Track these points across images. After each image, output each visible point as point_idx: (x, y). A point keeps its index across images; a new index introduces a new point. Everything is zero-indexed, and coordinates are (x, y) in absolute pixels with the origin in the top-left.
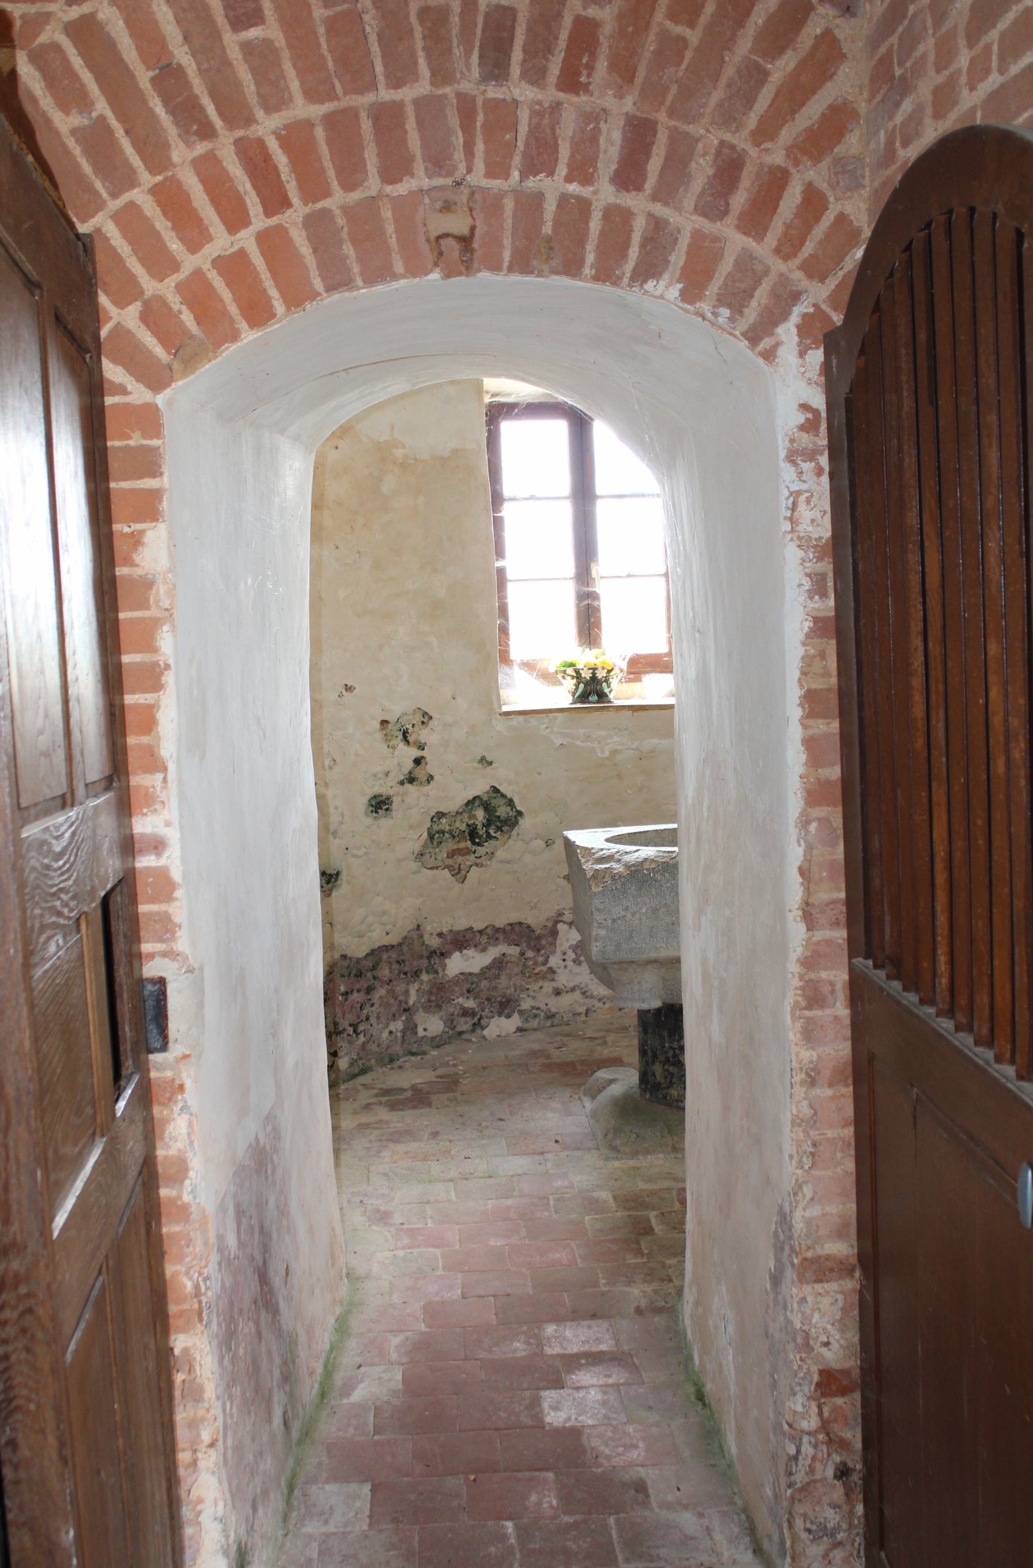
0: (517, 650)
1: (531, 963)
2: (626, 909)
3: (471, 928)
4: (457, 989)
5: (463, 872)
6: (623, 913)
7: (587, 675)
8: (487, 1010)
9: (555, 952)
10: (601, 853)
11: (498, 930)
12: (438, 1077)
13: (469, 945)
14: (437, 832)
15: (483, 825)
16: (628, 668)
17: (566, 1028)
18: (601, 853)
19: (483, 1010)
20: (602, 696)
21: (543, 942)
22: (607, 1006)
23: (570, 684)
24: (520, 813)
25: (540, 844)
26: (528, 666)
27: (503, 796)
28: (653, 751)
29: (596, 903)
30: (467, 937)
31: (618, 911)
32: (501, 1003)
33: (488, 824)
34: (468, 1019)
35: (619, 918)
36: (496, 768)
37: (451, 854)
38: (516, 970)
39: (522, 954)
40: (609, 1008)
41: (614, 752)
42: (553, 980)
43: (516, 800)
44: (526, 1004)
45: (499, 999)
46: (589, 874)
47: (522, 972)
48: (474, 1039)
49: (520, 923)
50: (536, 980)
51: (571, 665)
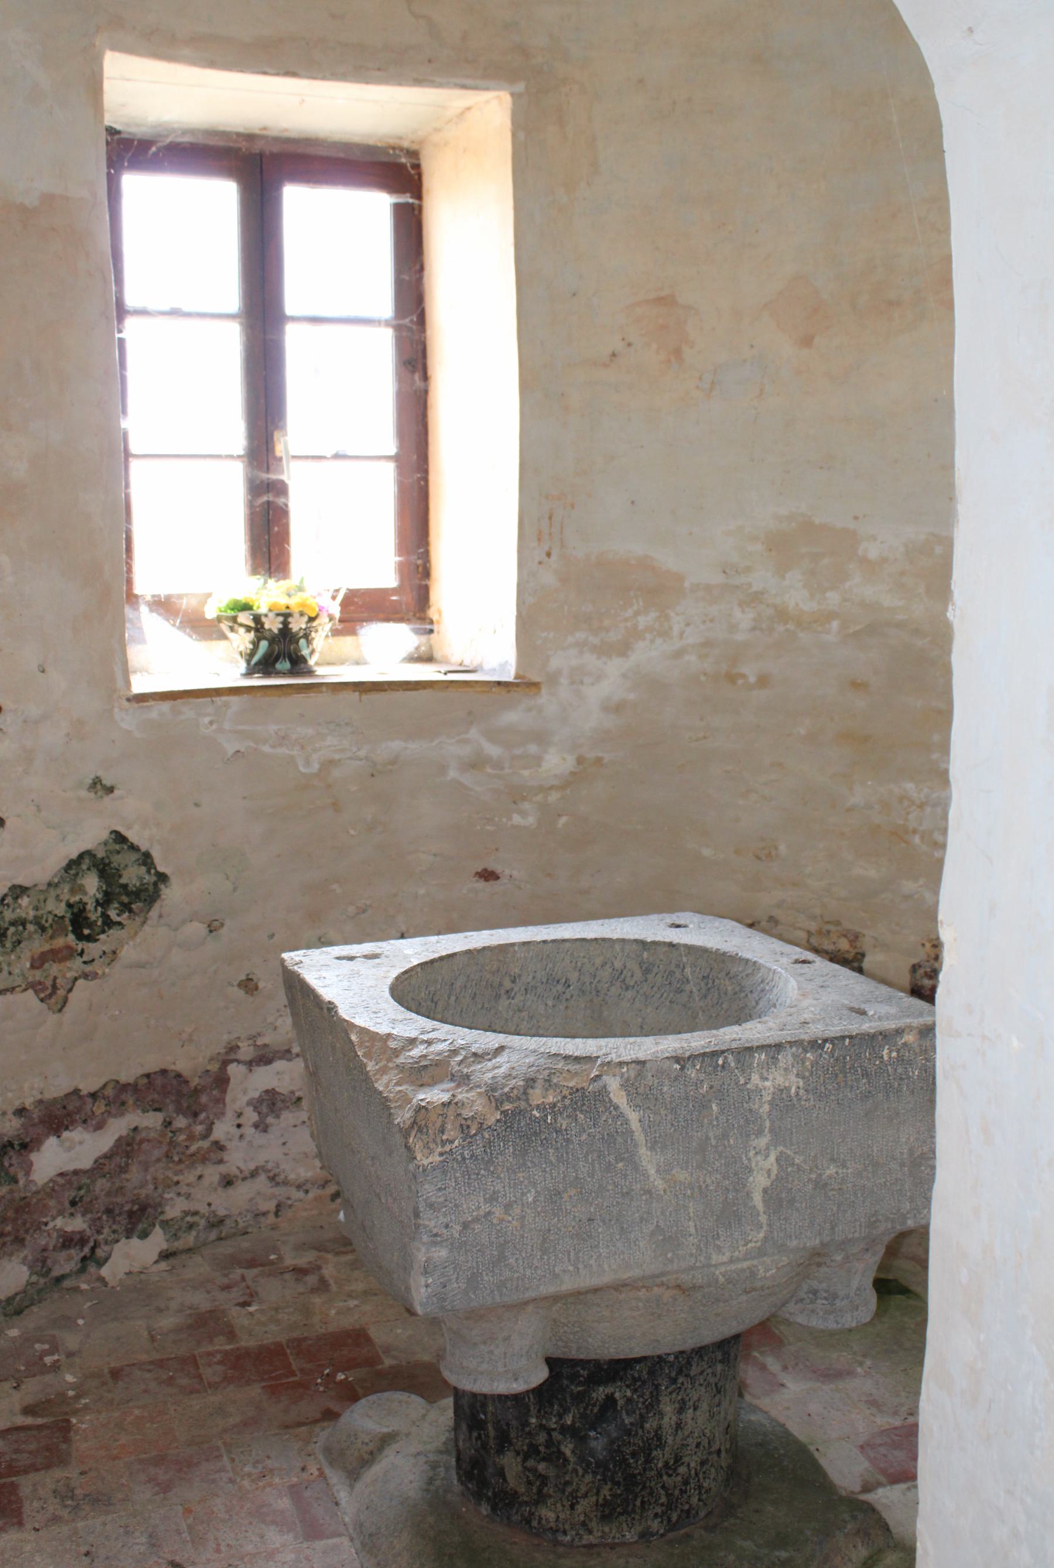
0: (144, 584)
1: (182, 1137)
2: (493, 1199)
3: (76, 1092)
4: (52, 1203)
5: (61, 992)
6: (485, 1208)
7: (273, 625)
8: (106, 1230)
9: (223, 1114)
10: (416, 1052)
11: (124, 1088)
12: (28, 1411)
13: (73, 1122)
14: (13, 923)
15: (97, 902)
16: (342, 612)
17: (245, 1243)
18: (416, 1052)
19: (99, 1232)
20: (298, 664)
21: (204, 1099)
22: (311, 1195)
23: (243, 640)
24: (163, 878)
25: (198, 928)
26: (164, 606)
27: (133, 848)
28: (394, 762)
29: (429, 1190)
30: (70, 1107)
31: (474, 1205)
32: (131, 1214)
33: (105, 902)
34: (73, 1251)
35: (476, 1220)
36: (122, 798)
37: (38, 962)
38: (157, 1153)
39: (167, 1124)
40: (316, 1199)
41: (329, 764)
42: (221, 1161)
43: (156, 855)
44: (174, 1210)
45: (127, 1208)
46: (403, 1117)
47: (168, 1156)
48: (84, 1286)
49: (164, 1072)
50: (192, 1166)
51: (246, 607)
